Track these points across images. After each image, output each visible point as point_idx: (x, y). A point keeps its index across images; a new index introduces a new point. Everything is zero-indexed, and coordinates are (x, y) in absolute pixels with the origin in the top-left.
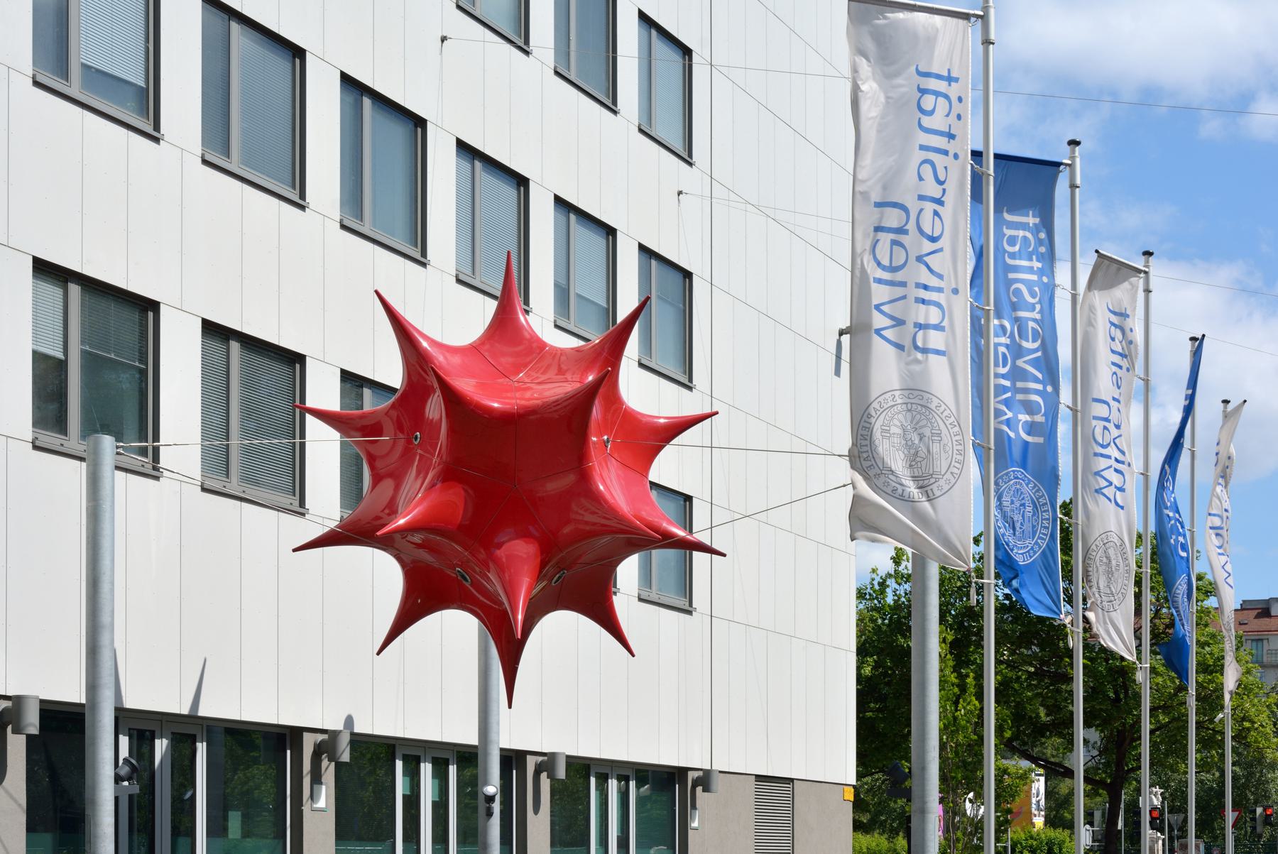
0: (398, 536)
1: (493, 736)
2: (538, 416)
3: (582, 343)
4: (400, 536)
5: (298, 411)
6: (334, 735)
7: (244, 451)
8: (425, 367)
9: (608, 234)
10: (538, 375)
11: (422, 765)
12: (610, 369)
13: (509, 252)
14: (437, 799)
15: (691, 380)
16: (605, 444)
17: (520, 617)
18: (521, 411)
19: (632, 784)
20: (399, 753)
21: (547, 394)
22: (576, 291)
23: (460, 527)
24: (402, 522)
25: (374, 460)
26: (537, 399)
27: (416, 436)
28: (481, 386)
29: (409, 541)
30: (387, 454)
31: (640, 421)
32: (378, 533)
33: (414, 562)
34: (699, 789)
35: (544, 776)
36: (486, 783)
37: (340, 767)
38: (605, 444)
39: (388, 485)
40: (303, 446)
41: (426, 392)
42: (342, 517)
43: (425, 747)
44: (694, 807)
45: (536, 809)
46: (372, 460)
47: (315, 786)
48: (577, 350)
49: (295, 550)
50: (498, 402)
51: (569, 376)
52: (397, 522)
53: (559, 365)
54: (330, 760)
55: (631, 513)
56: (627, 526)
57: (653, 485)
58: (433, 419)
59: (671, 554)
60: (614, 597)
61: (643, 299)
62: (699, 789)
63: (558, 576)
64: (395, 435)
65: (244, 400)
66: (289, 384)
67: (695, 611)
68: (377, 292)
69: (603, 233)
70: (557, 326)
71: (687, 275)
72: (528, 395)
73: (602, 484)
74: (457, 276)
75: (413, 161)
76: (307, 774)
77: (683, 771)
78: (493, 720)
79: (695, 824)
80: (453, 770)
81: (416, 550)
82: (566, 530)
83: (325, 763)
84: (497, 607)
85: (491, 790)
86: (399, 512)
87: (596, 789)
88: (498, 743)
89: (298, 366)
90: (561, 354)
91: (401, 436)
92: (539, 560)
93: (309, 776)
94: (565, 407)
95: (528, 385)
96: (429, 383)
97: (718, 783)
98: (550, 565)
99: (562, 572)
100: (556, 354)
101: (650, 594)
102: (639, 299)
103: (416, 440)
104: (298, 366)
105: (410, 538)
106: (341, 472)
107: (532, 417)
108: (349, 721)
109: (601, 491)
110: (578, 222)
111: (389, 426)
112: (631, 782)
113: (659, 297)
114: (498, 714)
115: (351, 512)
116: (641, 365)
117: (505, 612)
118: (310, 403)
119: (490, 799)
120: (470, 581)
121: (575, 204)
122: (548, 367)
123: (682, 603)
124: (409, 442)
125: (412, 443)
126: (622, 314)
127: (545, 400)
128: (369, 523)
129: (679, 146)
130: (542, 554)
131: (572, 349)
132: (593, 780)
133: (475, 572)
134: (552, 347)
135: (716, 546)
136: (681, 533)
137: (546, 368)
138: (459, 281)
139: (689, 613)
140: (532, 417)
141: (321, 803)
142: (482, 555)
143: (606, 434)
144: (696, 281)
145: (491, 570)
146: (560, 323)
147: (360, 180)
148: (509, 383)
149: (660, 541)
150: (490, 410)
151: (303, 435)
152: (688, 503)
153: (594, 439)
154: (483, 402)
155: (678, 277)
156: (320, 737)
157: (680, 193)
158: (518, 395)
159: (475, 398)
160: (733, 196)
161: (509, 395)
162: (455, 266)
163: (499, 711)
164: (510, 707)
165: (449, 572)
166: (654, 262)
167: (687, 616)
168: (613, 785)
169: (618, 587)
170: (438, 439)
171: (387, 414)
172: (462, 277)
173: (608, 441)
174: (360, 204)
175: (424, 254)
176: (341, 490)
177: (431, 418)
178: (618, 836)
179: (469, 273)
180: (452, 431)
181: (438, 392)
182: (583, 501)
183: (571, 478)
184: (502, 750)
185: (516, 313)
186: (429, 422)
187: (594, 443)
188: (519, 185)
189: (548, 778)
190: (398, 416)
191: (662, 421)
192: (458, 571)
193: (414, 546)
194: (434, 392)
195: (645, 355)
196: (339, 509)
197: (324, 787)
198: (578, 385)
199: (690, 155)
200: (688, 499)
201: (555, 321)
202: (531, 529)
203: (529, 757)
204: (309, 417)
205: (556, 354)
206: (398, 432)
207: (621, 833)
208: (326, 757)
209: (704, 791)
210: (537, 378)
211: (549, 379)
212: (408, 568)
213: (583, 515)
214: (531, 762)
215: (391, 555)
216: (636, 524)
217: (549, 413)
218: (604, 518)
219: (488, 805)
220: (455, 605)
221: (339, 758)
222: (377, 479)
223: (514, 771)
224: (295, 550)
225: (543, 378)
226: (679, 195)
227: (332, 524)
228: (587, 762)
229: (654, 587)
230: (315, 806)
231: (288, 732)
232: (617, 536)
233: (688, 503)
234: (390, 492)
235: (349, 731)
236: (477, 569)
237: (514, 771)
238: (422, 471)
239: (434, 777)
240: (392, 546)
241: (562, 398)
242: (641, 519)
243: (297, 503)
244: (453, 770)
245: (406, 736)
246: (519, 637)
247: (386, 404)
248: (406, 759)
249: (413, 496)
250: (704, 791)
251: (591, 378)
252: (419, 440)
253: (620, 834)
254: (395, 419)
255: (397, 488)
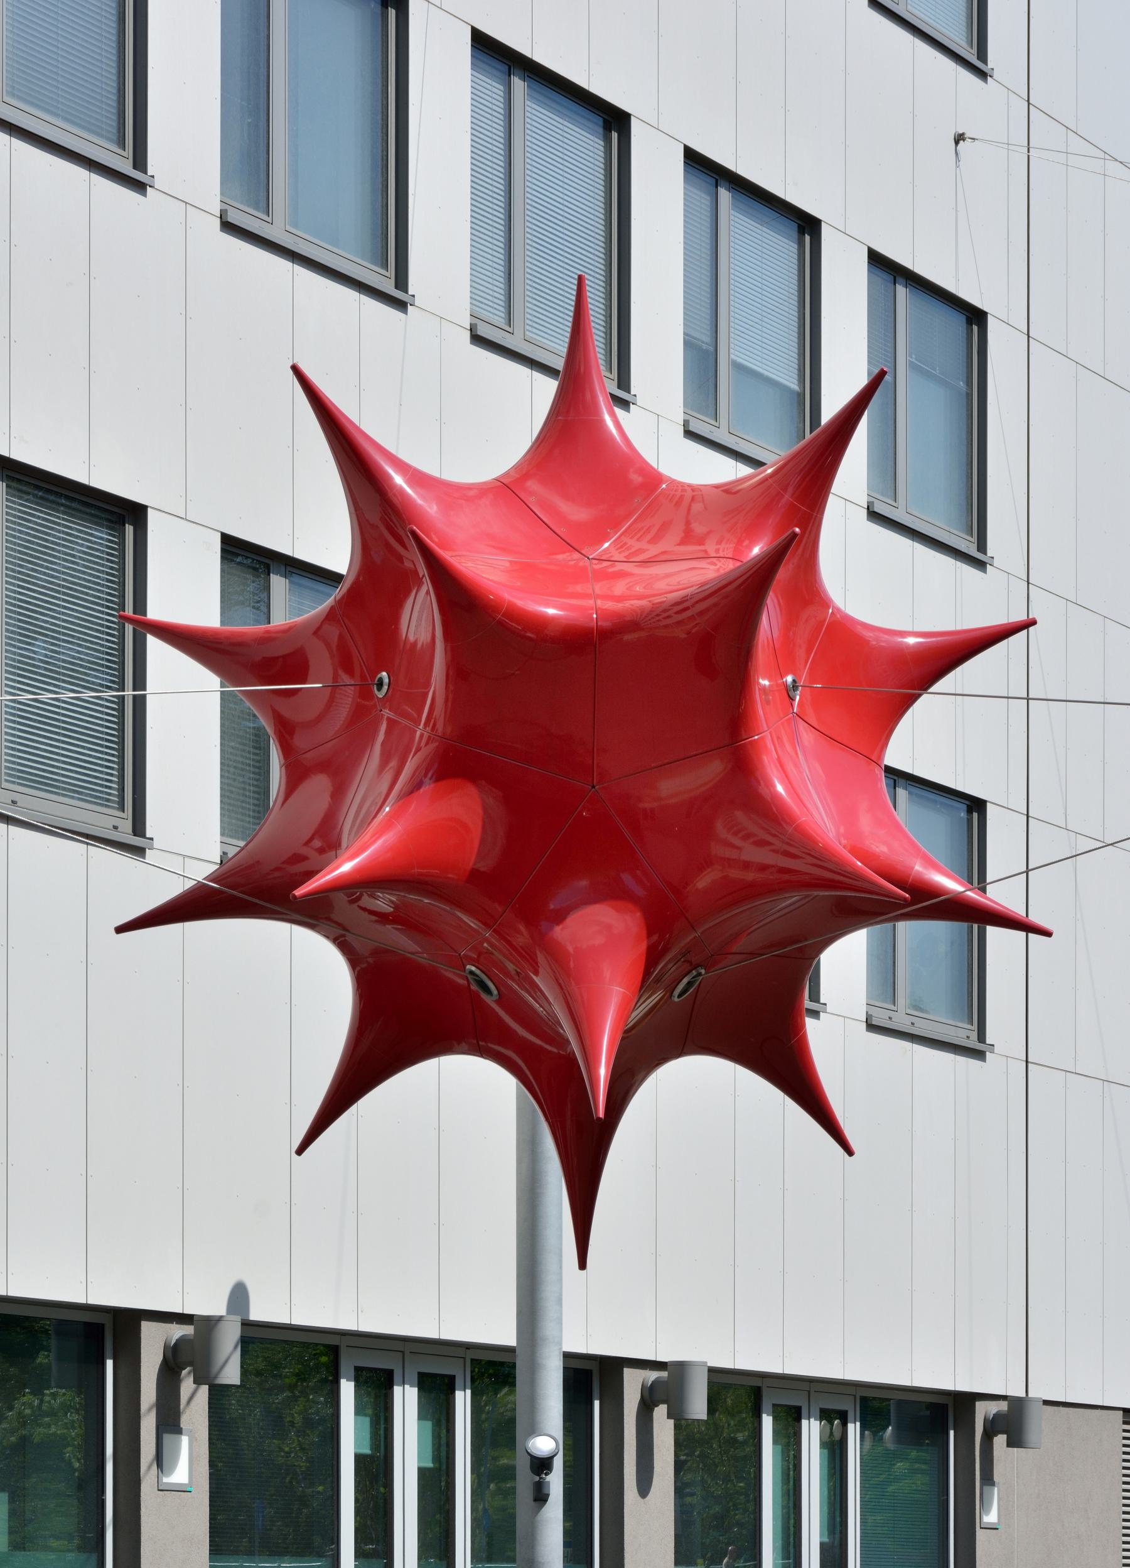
0: (341, 898)
1: (548, 1328)
2: (643, 634)
3: (744, 470)
4: (346, 898)
5: (129, 629)
6: (207, 1325)
7: (14, 715)
8: (401, 532)
9: (801, 231)
10: (643, 544)
11: (397, 1390)
12: (797, 530)
13: (581, 279)
14: (430, 1465)
15: (982, 546)
16: (788, 693)
17: (603, 1072)
18: (605, 624)
19: (853, 1430)
20: (347, 1365)
21: (661, 585)
22: (732, 356)
23: (474, 876)
24: (347, 867)
25: (291, 733)
26: (640, 597)
27: (381, 681)
28: (524, 570)
29: (364, 909)
30: (319, 719)
31: (860, 641)
32: (298, 892)
33: (376, 952)
34: (1000, 1440)
35: (660, 1412)
36: (534, 1430)
37: (219, 1395)
38: (788, 693)
39: (318, 786)
40: (140, 704)
41: (404, 585)
42: (225, 853)
43: (403, 1352)
44: (988, 1479)
45: (644, 1486)
46: (286, 730)
47: (167, 1438)
48: (727, 489)
49: (121, 929)
50: (554, 607)
51: (711, 547)
52: (337, 868)
53: (688, 523)
54: (198, 1381)
55: (844, 842)
56: (835, 872)
57: (897, 776)
58: (416, 642)
59: (940, 931)
60: (809, 1022)
61: (876, 371)
62: (1000, 1440)
63: (685, 981)
64: (335, 678)
65: (14, 605)
66: (112, 568)
67: (992, 1052)
68: (296, 369)
69: (792, 228)
70: (689, 434)
71: (976, 317)
72: (620, 588)
73: (781, 783)
74: (472, 329)
75: (379, 81)
76: (150, 1410)
77: (965, 1401)
78: (548, 1292)
79: (991, 1518)
80: (463, 1400)
81: (379, 927)
82: (703, 882)
83: (187, 1385)
84: (555, 1050)
85: (544, 1444)
86: (344, 844)
87: (775, 1442)
88: (560, 1343)
89: (129, 530)
90: (693, 499)
91: (345, 679)
92: (643, 946)
93: (153, 1414)
94: (701, 613)
95: (619, 567)
96: (408, 564)
97: (1040, 1424)
98: (669, 956)
99: (694, 973)
100: (682, 497)
101: (891, 1014)
102: (869, 373)
103: (379, 689)
104: (129, 530)
105: (366, 901)
106: (222, 757)
107: (627, 637)
108: (239, 1296)
109: (776, 795)
110: (735, 207)
111: (321, 659)
112: (851, 1426)
113: (913, 367)
114: (560, 1280)
115: (242, 844)
116: (874, 516)
117: (571, 1060)
118: (154, 613)
119: (542, 1465)
120: (495, 992)
121: (731, 167)
122: (664, 527)
123: (964, 1034)
124: (365, 692)
125: (371, 696)
126: (831, 407)
127: (657, 600)
128: (277, 869)
129: (957, 37)
130: (649, 935)
131: (717, 487)
132: (767, 1422)
133: (507, 974)
134: (673, 482)
135: (1035, 918)
136: (952, 885)
137: (659, 530)
138: (478, 339)
139: (979, 1055)
140: (627, 637)
141: (180, 1475)
142: (522, 936)
143: (787, 674)
144: (994, 329)
145: (541, 970)
146: (696, 427)
147: (263, 124)
148: (581, 564)
149: (906, 903)
150: (539, 624)
151: (140, 681)
152: (975, 815)
153: (765, 682)
154: (520, 603)
155: (956, 321)
156: (177, 1331)
157: (959, 138)
158: (598, 588)
159: (506, 596)
160: (1076, 144)
161: (579, 588)
162: (468, 306)
163: (560, 1274)
164: (582, 1265)
165: (449, 974)
166: (901, 291)
167: (973, 1063)
168: (812, 1431)
169: (822, 1001)
170: (427, 685)
171: (316, 632)
172: (484, 331)
173: (795, 686)
174: (263, 176)
175: (401, 281)
176: (222, 796)
177: (412, 638)
178: (822, 1545)
179: (500, 321)
180: (458, 672)
181: (427, 586)
182: (739, 815)
183: (713, 770)
184: (567, 1356)
185: (597, 412)
186: (408, 647)
187: (764, 689)
188: (607, 128)
189: (669, 1417)
190: (341, 636)
191: (911, 640)
192: (471, 972)
193: (374, 918)
194: (420, 584)
195: (882, 494)
196: (217, 837)
197: (185, 1440)
198: (730, 566)
199: (982, 54)
200: (977, 806)
201: (686, 423)
202: (627, 878)
203: (628, 1372)
204: (154, 644)
205: (682, 497)
206: (340, 672)
207: (829, 1534)
208: (189, 1373)
209: (1010, 1444)
210: (640, 551)
211: (664, 553)
212: (364, 966)
213: (739, 848)
214: (633, 1383)
215: (327, 937)
216: (858, 866)
217: (666, 626)
218: (787, 854)
219: (537, 1478)
220: (464, 1046)
221: (216, 1377)
222: (296, 775)
223: (597, 1404)
224: (120, 930)
225: (653, 551)
226: (957, 143)
227: (201, 872)
228: (756, 1382)
229: (901, 1000)
230: (165, 1480)
231: (106, 1320)
232: (816, 893)
233: (975, 815)
234: (322, 803)
235: (239, 1318)
236: (511, 967)
237: (597, 1404)
238: (394, 754)
239: (421, 1416)
240: (329, 919)
241: (693, 595)
242: (856, 851)
243: (127, 825)
244: (463, 1400)
245: (364, 1328)
246: (601, 1115)
247: (320, 608)
248: (363, 1377)
249: (374, 809)
250: (1010, 1444)
251: (756, 550)
252: (385, 687)
253: (826, 1540)
254: (334, 642)
255: (339, 792)
